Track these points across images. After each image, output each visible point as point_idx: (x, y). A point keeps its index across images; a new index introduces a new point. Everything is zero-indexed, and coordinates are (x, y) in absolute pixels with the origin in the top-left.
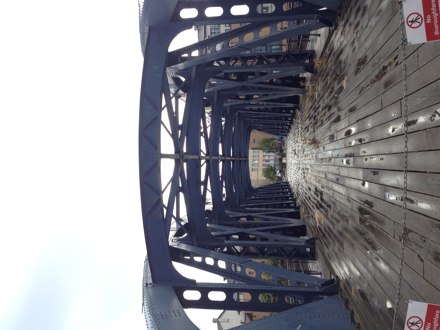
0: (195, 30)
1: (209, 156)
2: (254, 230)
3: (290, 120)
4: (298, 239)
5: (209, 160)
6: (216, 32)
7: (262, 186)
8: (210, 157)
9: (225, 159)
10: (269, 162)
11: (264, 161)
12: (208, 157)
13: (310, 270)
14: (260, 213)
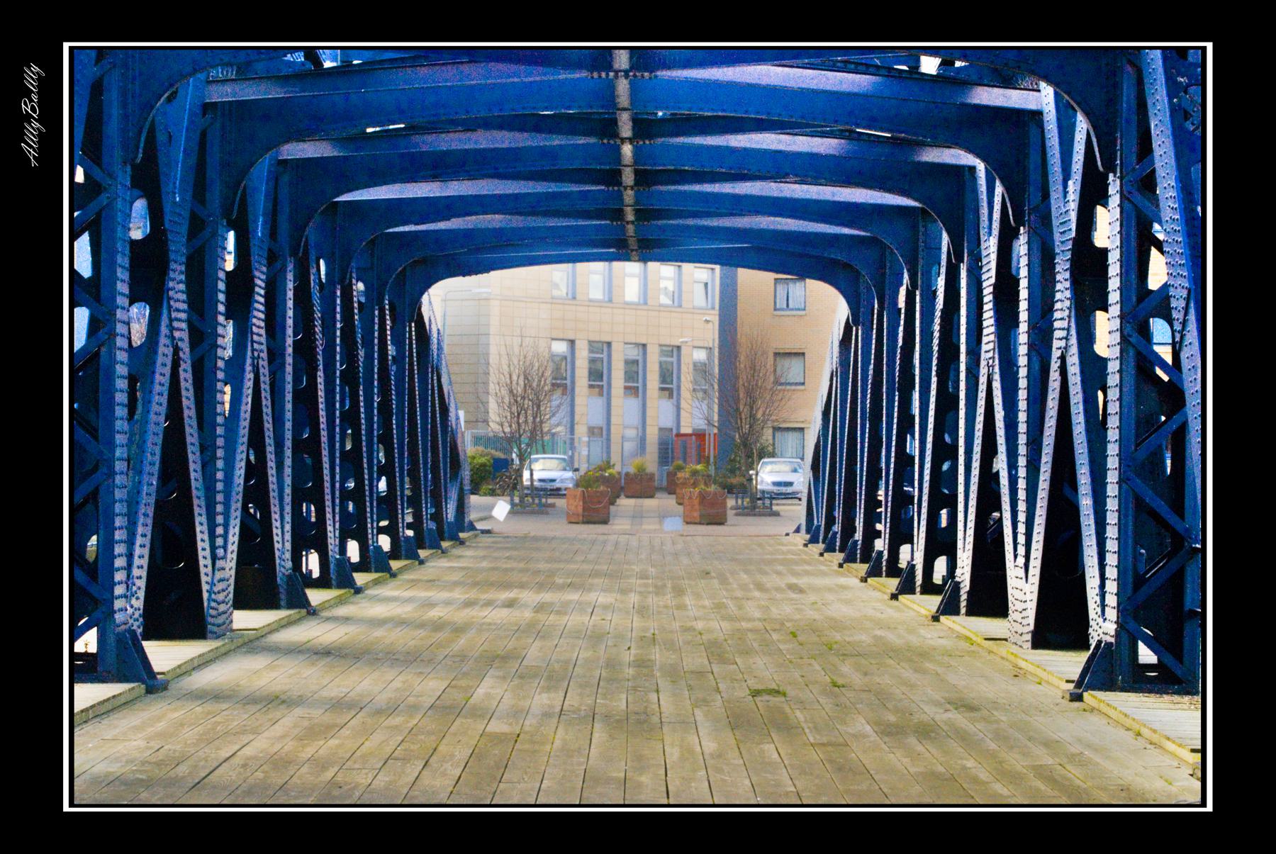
2: (177, 334)
9: (617, 72)
10: (622, 391)
11: (634, 353)
14: (264, 355)
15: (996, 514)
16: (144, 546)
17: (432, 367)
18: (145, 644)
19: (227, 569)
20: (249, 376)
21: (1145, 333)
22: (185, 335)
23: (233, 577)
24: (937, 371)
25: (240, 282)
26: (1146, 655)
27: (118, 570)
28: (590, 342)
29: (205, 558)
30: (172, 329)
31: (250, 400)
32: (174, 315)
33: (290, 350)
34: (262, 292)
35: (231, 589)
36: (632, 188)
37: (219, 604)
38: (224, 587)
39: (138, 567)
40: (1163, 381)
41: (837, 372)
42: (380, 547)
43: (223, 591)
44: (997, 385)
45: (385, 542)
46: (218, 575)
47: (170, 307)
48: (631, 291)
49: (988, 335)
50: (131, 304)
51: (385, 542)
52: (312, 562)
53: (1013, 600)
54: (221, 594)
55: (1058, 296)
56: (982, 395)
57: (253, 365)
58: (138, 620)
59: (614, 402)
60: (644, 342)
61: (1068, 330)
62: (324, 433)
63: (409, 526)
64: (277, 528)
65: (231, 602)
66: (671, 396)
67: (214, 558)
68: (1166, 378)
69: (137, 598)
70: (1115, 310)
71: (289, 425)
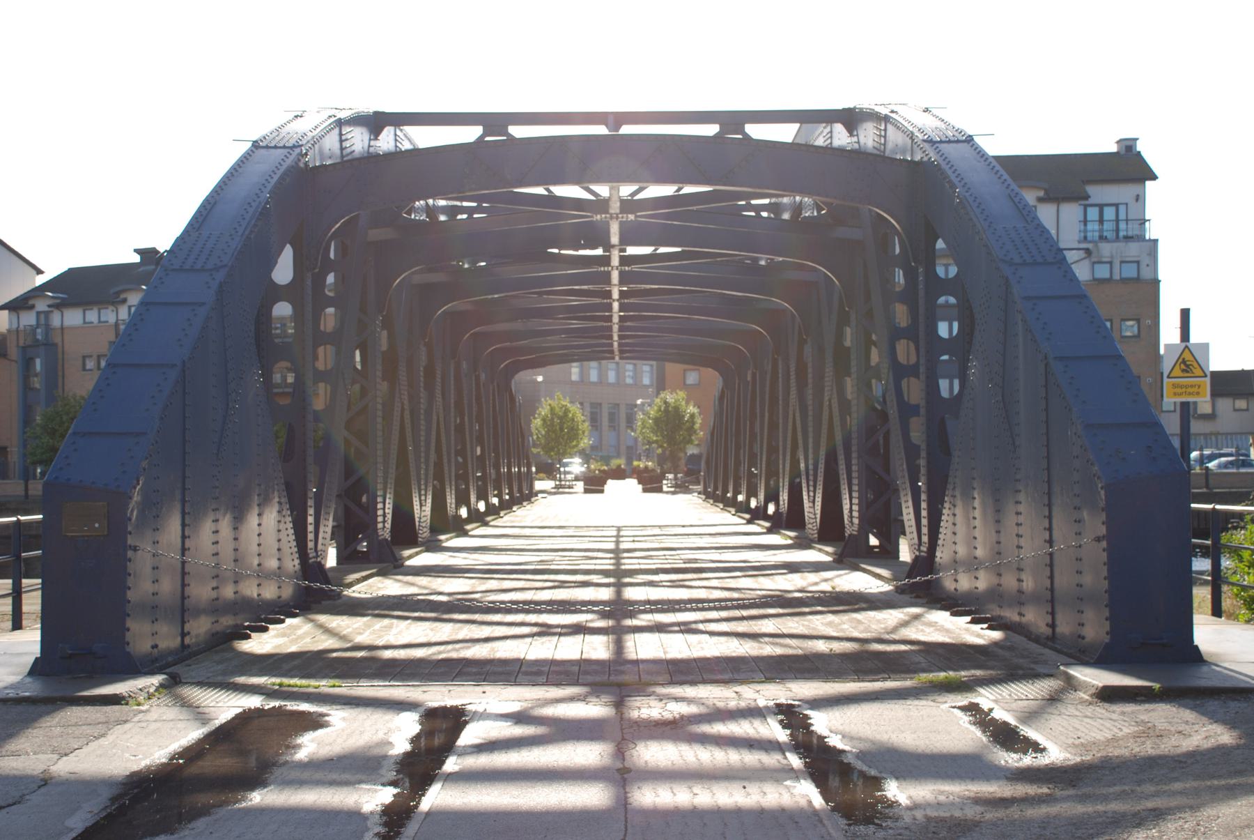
0: (1118, 142)
1: (618, 211)
2: (403, 397)
5: (607, 212)
6: (1103, 225)
8: (617, 214)
12: (615, 207)
13: (850, 426)
14: (441, 407)
21: (869, 386)
22: (406, 397)
26: (873, 541)
33: (452, 405)
35: (429, 521)
42: (478, 509)
44: (798, 415)
45: (482, 506)
46: (423, 514)
48: (594, 376)
51: (495, 501)
56: (790, 420)
63: (508, 494)
66: (614, 430)
70: (854, 376)
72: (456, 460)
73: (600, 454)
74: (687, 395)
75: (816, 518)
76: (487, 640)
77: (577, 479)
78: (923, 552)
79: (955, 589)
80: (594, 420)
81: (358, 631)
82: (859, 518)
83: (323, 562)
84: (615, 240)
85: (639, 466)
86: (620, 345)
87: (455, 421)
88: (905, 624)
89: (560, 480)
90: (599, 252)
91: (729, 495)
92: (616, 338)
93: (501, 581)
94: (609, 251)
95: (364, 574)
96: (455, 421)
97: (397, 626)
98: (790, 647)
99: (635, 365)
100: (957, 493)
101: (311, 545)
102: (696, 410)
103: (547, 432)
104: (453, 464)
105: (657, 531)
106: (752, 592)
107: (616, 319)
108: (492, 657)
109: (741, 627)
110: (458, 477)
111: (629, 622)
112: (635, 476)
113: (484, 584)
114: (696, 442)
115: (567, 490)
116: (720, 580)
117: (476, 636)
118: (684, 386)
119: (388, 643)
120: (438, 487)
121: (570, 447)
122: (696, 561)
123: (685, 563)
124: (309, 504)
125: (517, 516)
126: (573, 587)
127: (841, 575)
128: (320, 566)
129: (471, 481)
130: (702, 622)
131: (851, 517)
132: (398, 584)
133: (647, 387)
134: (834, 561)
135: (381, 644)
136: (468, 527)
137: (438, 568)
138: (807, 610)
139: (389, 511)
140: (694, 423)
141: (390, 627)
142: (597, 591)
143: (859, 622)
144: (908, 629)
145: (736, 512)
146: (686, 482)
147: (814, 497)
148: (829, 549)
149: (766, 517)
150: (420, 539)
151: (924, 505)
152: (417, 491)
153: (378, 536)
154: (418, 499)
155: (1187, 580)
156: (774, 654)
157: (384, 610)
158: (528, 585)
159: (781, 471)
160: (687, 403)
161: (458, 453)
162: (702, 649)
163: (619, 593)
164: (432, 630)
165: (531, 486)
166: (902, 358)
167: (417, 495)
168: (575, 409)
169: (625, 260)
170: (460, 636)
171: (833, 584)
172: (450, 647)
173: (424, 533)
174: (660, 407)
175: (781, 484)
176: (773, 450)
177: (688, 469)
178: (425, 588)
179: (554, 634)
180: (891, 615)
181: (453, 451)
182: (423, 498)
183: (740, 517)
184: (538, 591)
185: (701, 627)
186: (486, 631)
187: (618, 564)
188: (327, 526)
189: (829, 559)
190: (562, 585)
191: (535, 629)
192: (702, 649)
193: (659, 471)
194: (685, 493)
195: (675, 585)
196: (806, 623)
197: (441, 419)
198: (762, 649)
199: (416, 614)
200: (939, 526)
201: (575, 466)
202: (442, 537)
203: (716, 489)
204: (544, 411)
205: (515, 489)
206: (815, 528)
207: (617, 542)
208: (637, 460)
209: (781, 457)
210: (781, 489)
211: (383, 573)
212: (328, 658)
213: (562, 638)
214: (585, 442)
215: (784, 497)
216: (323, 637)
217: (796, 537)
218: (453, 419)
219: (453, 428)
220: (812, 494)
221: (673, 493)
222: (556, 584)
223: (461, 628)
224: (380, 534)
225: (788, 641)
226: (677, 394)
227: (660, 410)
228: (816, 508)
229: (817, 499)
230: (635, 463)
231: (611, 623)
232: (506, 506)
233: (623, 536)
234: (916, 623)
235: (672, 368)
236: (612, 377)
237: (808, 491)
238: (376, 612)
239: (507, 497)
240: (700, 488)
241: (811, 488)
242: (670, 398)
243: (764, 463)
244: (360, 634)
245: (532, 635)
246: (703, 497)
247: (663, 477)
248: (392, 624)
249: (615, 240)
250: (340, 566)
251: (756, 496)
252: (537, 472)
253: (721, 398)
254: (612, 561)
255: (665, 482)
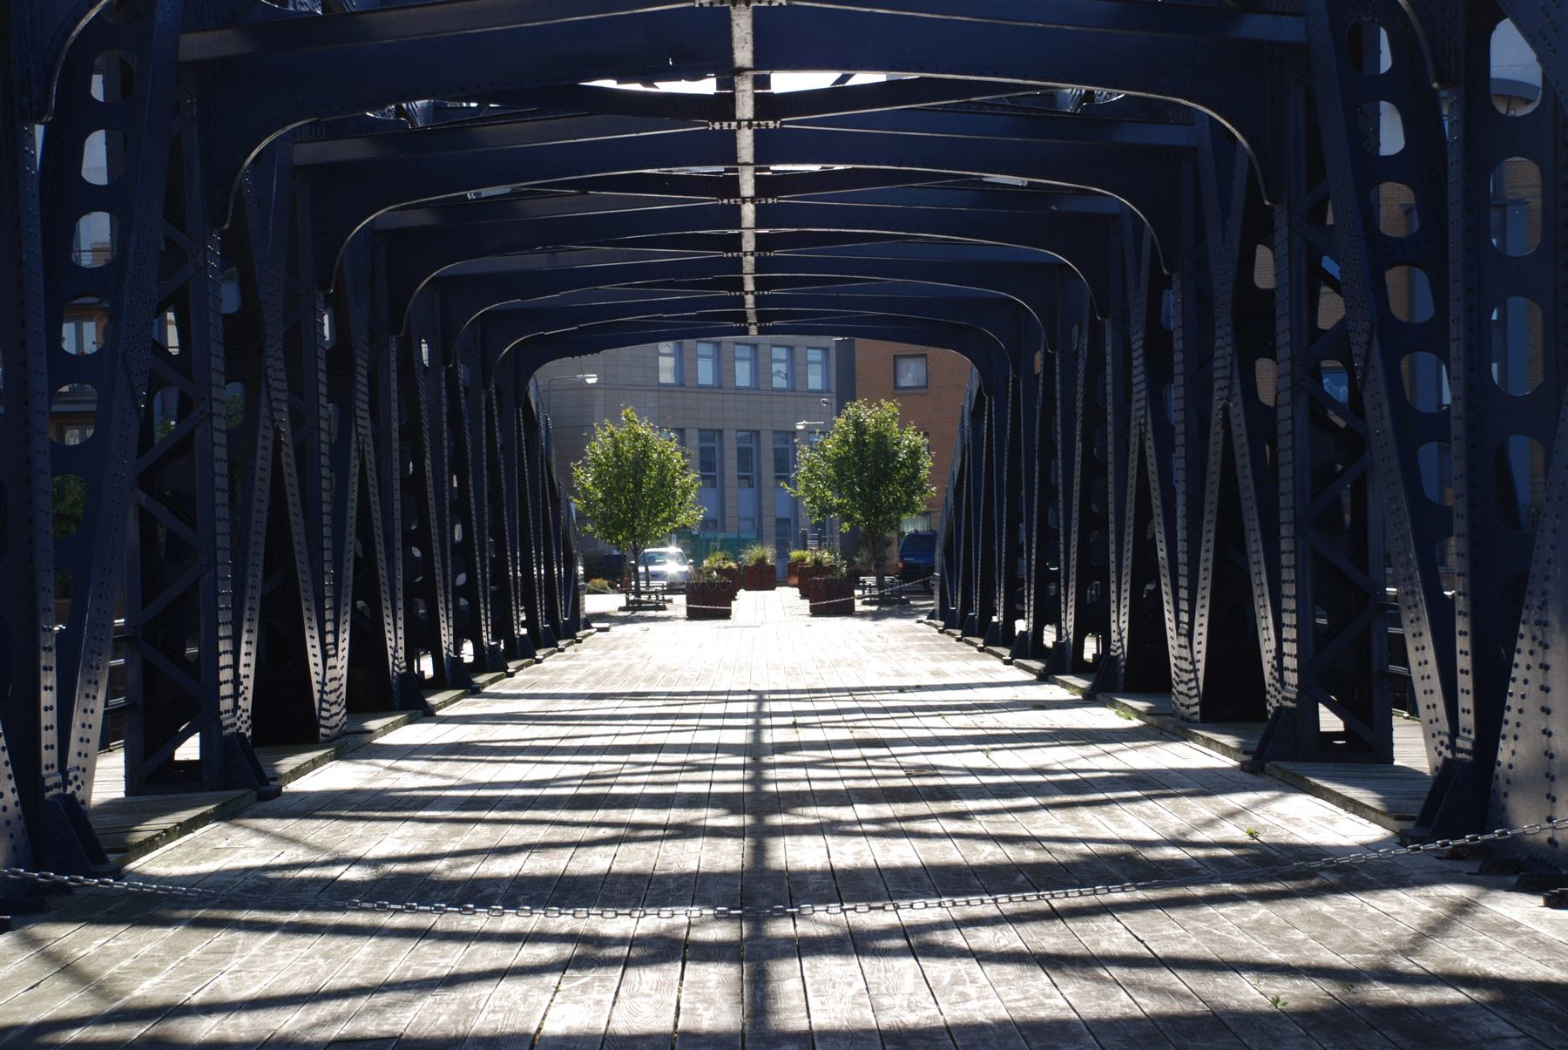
2: (277, 416)
3: (1079, 646)
4: (247, 688)
7: (548, 437)
9: (739, 122)
10: (736, 481)
14: (369, 440)
15: (1150, 587)
16: (250, 654)
17: (542, 457)
18: (255, 750)
19: (339, 667)
20: (355, 462)
23: (345, 676)
24: (1081, 436)
25: (341, 356)
26: (1329, 721)
27: (224, 698)
28: (700, 430)
29: (315, 656)
30: (272, 410)
31: (356, 488)
32: (274, 395)
33: (396, 435)
34: (365, 373)
35: (343, 689)
36: (752, 254)
37: (331, 704)
38: (337, 687)
39: (245, 665)
40: (1340, 428)
41: (969, 446)
43: (335, 690)
46: (330, 674)
47: (268, 386)
49: (1138, 392)
50: (227, 382)
52: (426, 665)
53: (1177, 671)
54: (333, 694)
55: (1218, 343)
56: (1133, 457)
57: (358, 449)
58: (246, 722)
59: (728, 492)
60: (757, 429)
61: (1231, 378)
62: (434, 524)
63: (524, 624)
64: (389, 624)
65: (344, 703)
67: (325, 656)
68: (1342, 424)
69: (245, 699)
70: (1284, 353)
71: (398, 515)
72: (407, 555)
73: (721, 536)
74: (900, 409)
75: (1195, 671)
76: (453, 981)
77: (673, 589)
78: (1462, 750)
79: (1551, 841)
80: (708, 465)
81: (147, 965)
82: (1299, 670)
83: (79, 795)
84: (743, 55)
85: (803, 559)
86: (759, 301)
87: (404, 468)
88: (1438, 927)
89: (638, 593)
90: (707, 86)
91: (995, 619)
92: (749, 285)
93: (499, 827)
94: (732, 85)
95: (184, 816)
96: (404, 468)
97: (245, 948)
98: (1174, 994)
99: (791, 348)
100: (1553, 618)
101: (49, 757)
102: (920, 440)
103: (608, 493)
104: (400, 565)
105: (846, 703)
106: (1066, 847)
107: (749, 243)
108: (461, 1028)
109: (1050, 938)
110: (411, 592)
111: (783, 928)
112: (795, 580)
113: (460, 834)
114: (924, 508)
115: (652, 613)
116: (992, 818)
117: (431, 972)
118: (896, 391)
119: (216, 997)
120: (367, 613)
121: (656, 523)
122: (933, 770)
123: (909, 776)
124: (43, 663)
125: (544, 672)
126: (661, 838)
127: (1264, 802)
128: (74, 809)
129: (441, 599)
130: (959, 924)
131: (1280, 668)
132: (257, 841)
133: (819, 393)
134: (1243, 767)
135: (196, 1000)
136: (434, 700)
137: (359, 799)
138: (1200, 891)
139: (247, 670)
140: (917, 469)
141: (228, 952)
142: (716, 848)
143: (1328, 921)
144: (1451, 942)
145: (1014, 656)
146: (901, 592)
147: (1191, 623)
148: (1229, 740)
149: (1080, 668)
150: (322, 730)
151: (1463, 643)
152: (315, 624)
153: (222, 728)
154: (317, 642)
155: (73, 383)
156: (1138, 1013)
157: (215, 907)
158: (558, 834)
159: (1113, 567)
160: (902, 426)
161: (409, 539)
162: (965, 997)
163: (759, 852)
164: (326, 956)
165: (576, 605)
166: (1398, 309)
167: (316, 633)
168: (666, 447)
169: (768, 105)
170: (392, 972)
171: (1250, 826)
172: (362, 1002)
173: (333, 714)
174: (846, 434)
175: (1113, 597)
176: (1093, 523)
177: (906, 565)
178: (311, 847)
179: (612, 962)
180: (1401, 903)
181: (398, 535)
182: (330, 638)
183: (1021, 667)
184: (581, 851)
185: (956, 938)
186: (452, 958)
187: (758, 781)
188: (92, 710)
189: (1229, 762)
190: (634, 834)
191: (568, 950)
192: (965, 997)
193: (844, 570)
194: (900, 616)
195: (887, 830)
196: (1203, 926)
197: (371, 466)
198: (1107, 997)
199: (294, 917)
200: (1504, 693)
201: (671, 563)
202: (374, 725)
203: (967, 606)
204: (599, 446)
205: (541, 614)
206: (1194, 692)
207: (757, 729)
208: (797, 547)
209: (1112, 537)
210: (1113, 607)
211: (228, 814)
212: (57, 1045)
213: (632, 973)
214: (692, 515)
215: (1120, 623)
216: (60, 984)
217: (1150, 713)
218: (396, 465)
219: (397, 485)
220: (1184, 617)
221: (876, 616)
222: (622, 831)
223: (395, 951)
224: (226, 723)
225: (1165, 977)
226: (880, 406)
227: (845, 442)
228: (1196, 648)
229: (1197, 629)
230: (795, 554)
231: (748, 820)
232: (525, 651)
233: (771, 715)
234: (1466, 925)
235: (871, 352)
236: (743, 374)
237: (1177, 612)
238: (199, 913)
239: (524, 631)
240: (933, 604)
241: (1184, 605)
242: (868, 414)
243: (1074, 550)
244: (151, 972)
245: (561, 966)
246: (941, 623)
247: (853, 581)
248: (234, 943)
249: (743, 55)
250: (134, 798)
251: (1056, 621)
252: (587, 578)
253: (976, 414)
254: (748, 774)
255: (858, 592)
